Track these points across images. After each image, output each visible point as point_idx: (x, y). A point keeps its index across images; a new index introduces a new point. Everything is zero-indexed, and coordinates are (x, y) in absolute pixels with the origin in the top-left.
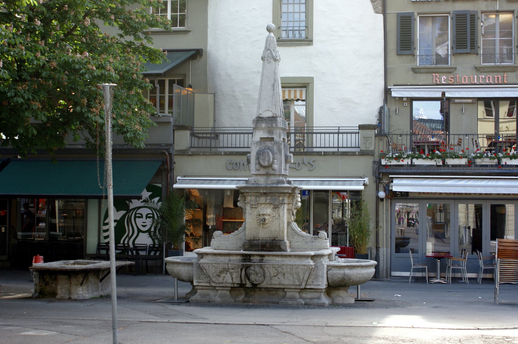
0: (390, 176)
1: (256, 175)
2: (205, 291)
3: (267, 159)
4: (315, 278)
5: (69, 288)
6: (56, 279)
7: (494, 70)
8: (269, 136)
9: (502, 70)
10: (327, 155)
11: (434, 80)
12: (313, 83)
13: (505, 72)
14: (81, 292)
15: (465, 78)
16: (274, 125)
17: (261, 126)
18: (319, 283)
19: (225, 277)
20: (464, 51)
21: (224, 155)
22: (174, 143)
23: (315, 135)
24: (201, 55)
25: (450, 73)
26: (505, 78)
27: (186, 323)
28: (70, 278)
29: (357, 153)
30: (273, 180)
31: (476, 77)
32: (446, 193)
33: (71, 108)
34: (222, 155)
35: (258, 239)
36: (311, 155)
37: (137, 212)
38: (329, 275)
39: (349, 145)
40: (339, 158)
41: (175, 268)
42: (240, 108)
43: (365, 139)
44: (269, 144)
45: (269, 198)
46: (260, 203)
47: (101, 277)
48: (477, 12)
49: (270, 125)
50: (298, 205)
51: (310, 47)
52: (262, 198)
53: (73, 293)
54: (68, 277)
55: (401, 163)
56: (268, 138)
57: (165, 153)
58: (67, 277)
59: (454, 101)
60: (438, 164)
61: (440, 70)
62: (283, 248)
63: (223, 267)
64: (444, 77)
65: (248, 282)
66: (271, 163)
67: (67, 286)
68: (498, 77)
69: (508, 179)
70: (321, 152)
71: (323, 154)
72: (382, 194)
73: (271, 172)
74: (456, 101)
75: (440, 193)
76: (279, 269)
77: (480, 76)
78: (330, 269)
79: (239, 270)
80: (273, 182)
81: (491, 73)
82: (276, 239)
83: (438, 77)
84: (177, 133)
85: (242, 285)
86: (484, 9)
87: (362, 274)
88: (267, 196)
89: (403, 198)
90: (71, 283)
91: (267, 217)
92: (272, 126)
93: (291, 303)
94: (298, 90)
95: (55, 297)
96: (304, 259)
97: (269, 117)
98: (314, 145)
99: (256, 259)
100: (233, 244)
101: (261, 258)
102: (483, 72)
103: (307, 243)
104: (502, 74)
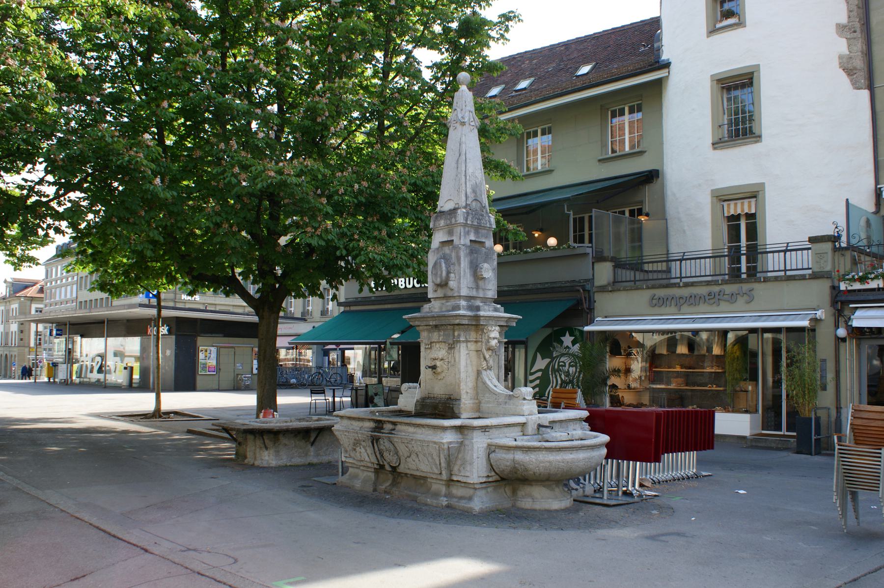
0: (851, 306)
3: (439, 273)
4: (461, 465)
10: (767, 281)
12: (764, 190)
14: (267, 458)
18: (468, 474)
21: (763, 282)
22: (593, 279)
24: (658, 177)
29: (807, 277)
37: (561, 360)
38: (492, 461)
39: (800, 267)
40: (784, 284)
42: (684, 231)
43: (819, 255)
45: (442, 333)
47: (312, 439)
50: (491, 344)
51: (758, 144)
55: (866, 286)
57: (579, 291)
66: (444, 278)
73: (450, 293)
78: (494, 451)
84: (597, 266)
87: (550, 462)
88: (439, 331)
91: (438, 363)
94: (746, 202)
98: (788, 267)
99: (388, 427)
103: (499, 404)
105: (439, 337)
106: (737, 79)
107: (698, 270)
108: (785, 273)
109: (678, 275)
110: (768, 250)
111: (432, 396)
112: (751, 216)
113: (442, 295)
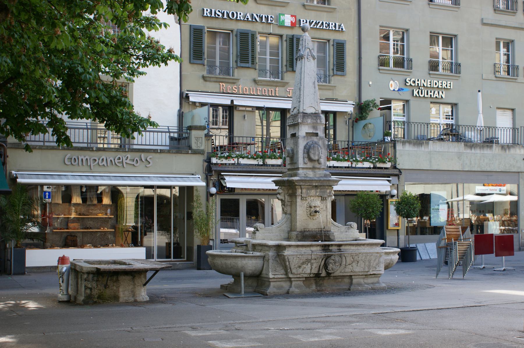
1: (303, 168)
2: (278, 283)
3: (317, 153)
6: (117, 280)
7: (269, 84)
8: (314, 132)
9: (275, 84)
11: (221, 89)
13: (277, 86)
15: (265, 90)
17: (307, 121)
19: (305, 268)
20: (247, 65)
25: (234, 83)
26: (277, 91)
27: (413, 311)
28: (134, 277)
30: (320, 174)
31: (254, 88)
32: (263, 189)
34: (60, 149)
35: (308, 230)
36: (148, 152)
39: (160, 144)
41: (239, 262)
44: (315, 139)
45: (319, 190)
46: (311, 195)
48: (255, 32)
49: (314, 121)
52: (313, 191)
53: (138, 295)
54: (131, 277)
56: (313, 133)
59: (238, 108)
60: (259, 164)
61: (227, 80)
62: (332, 238)
63: (306, 258)
64: (229, 86)
65: (324, 271)
68: (272, 91)
69: (255, 176)
71: (159, 151)
72: (213, 190)
73: (317, 166)
74: (241, 108)
75: (259, 189)
76: (356, 257)
77: (258, 89)
79: (320, 261)
80: (321, 175)
81: (266, 87)
83: (224, 86)
85: (317, 276)
86: (261, 30)
88: (317, 189)
89: (231, 193)
90: (134, 285)
92: (317, 122)
93: (361, 289)
95: (119, 301)
96: (374, 247)
97: (312, 113)
100: (277, 236)
101: (338, 248)
102: (261, 85)
104: (274, 88)
107: (81, 138)
108: (44, 144)
110: (98, 127)
112: (240, 33)
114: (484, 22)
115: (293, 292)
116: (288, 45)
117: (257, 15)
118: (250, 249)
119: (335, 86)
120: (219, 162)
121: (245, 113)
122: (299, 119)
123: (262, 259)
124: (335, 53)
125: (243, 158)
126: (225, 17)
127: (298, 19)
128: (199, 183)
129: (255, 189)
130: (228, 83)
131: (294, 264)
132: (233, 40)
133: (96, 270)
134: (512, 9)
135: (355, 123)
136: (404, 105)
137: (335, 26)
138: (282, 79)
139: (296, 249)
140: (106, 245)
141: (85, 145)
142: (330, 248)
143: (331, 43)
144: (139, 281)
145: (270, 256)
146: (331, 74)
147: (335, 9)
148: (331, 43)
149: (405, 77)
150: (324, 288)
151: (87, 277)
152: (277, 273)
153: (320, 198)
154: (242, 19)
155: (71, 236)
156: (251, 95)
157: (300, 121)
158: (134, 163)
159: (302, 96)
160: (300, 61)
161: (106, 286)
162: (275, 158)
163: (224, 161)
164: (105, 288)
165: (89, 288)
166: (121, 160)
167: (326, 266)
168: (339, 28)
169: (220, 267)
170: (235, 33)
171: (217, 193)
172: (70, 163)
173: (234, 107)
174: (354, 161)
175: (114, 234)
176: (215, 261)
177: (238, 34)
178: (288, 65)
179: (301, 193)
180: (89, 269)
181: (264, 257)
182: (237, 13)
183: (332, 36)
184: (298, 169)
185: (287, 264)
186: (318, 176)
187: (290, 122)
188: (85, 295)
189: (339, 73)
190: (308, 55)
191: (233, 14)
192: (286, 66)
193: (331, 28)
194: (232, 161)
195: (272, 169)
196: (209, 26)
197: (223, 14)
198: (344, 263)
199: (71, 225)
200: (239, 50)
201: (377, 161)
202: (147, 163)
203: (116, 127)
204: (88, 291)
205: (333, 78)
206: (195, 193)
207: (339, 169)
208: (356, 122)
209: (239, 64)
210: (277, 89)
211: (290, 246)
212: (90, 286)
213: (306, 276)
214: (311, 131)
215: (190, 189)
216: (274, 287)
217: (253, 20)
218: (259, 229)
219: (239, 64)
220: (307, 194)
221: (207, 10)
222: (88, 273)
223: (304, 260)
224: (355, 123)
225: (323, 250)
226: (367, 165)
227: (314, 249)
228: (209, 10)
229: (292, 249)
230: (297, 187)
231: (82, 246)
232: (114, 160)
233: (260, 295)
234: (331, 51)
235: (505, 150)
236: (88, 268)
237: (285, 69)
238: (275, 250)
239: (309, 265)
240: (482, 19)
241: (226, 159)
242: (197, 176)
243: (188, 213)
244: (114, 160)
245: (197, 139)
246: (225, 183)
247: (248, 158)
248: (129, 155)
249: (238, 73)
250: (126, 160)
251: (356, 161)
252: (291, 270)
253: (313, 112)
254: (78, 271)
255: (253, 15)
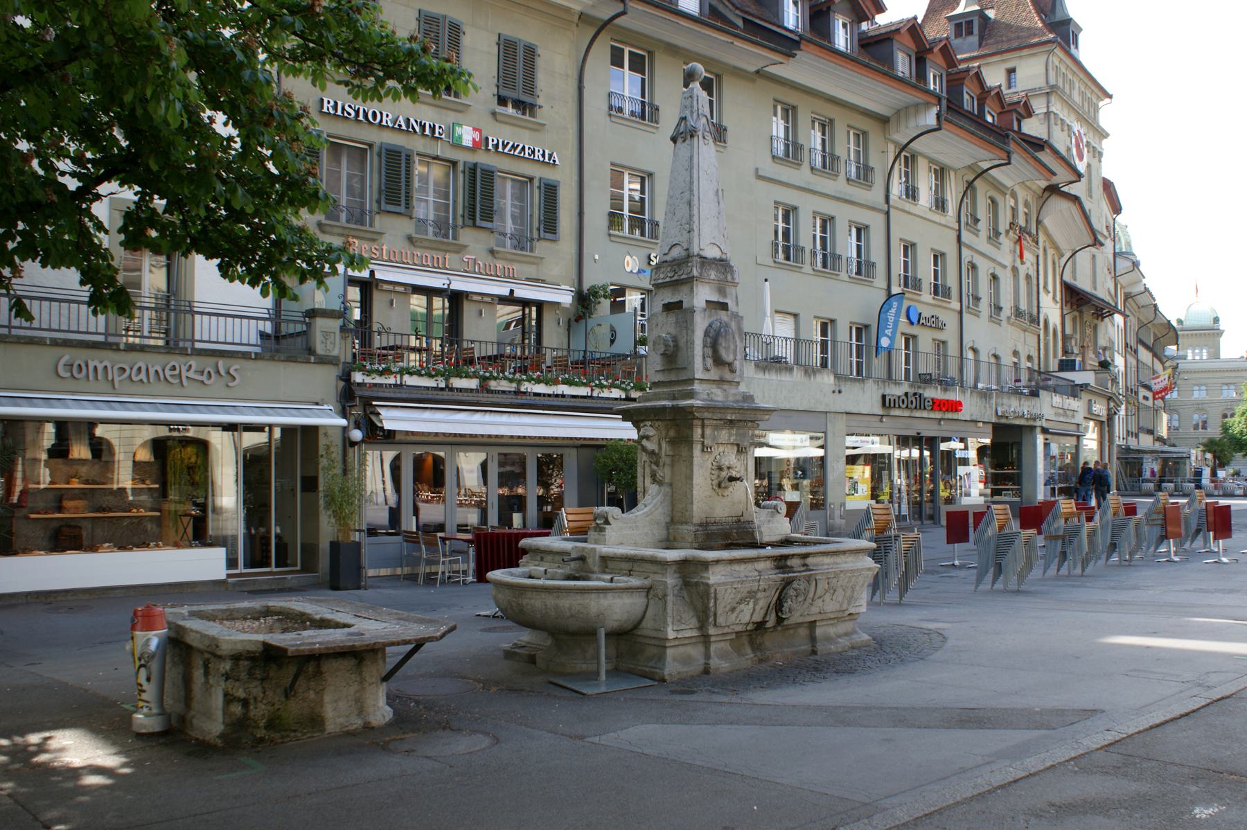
2: (681, 649)
3: (732, 347)
5: (358, 695)
6: (319, 673)
7: (434, 245)
8: (721, 300)
13: (446, 251)
16: (729, 278)
23: (197, 317)
25: (374, 240)
33: (189, 161)
34: (45, 344)
44: (723, 316)
45: (734, 432)
48: (412, 151)
58: (353, 661)
67: (355, 687)
70: (250, 353)
72: (357, 435)
73: (728, 376)
75: (437, 434)
76: (834, 580)
82: (742, 520)
85: (760, 626)
86: (421, 149)
88: (732, 428)
90: (362, 681)
95: (323, 730)
97: (715, 259)
98: (197, 337)
102: (421, 247)
105: (730, 437)
106: (451, 106)
108: (10, 332)
109: (190, 338)
111: (713, 520)
113: (717, 378)
114: (761, 173)
115: (717, 669)
116: (467, 179)
117: (416, 121)
118: (596, 569)
119: (542, 258)
120: (368, 380)
121: (393, 296)
122: (695, 269)
123: (644, 594)
124: (542, 202)
125: (411, 374)
126: (361, 117)
127: (484, 134)
128: (329, 419)
129: (430, 434)
130: (363, 238)
131: (723, 605)
132: (372, 162)
133: (261, 648)
134: (795, 157)
135: (573, 323)
136: (643, 299)
137: (543, 155)
138: (455, 238)
139: (728, 568)
140: (144, 545)
141: (101, 338)
142: (789, 563)
143: (536, 183)
144: (373, 671)
145: (669, 586)
146: (536, 235)
147: (543, 125)
148: (536, 183)
149: (648, 251)
150: (768, 653)
151: (232, 669)
152: (683, 627)
153: (735, 448)
154: (390, 125)
155: (70, 526)
156: (401, 264)
157: (695, 273)
158: (204, 378)
159: (696, 219)
160: (688, 141)
161: (289, 692)
162: (466, 377)
163: (378, 380)
164: (287, 696)
165: (239, 700)
166: (177, 372)
167: (779, 605)
168: (550, 159)
169: (539, 616)
170: (376, 149)
171: (363, 441)
172: (69, 374)
173: (374, 283)
174: (596, 386)
175: (158, 521)
176: (525, 602)
177: (383, 151)
178: (466, 215)
179: (703, 436)
180: (240, 647)
181: (648, 590)
182: (381, 114)
183: (537, 172)
184: (691, 381)
185: (712, 604)
186: (731, 398)
187: (662, 276)
188: (228, 720)
189: (548, 236)
190: (705, 130)
191: (374, 114)
192: (463, 216)
193: (536, 158)
194: (391, 380)
195: (461, 396)
196: (332, 131)
197: (357, 112)
198: (811, 595)
199: (68, 504)
200: (383, 181)
201: (632, 388)
202: (230, 378)
203: (249, 270)
204: (237, 709)
205: (538, 245)
206: (322, 441)
207: (542, 398)
208: (577, 321)
209: (384, 206)
210: (447, 257)
211: (717, 562)
212: (241, 693)
213: (739, 628)
214: (715, 298)
215: (310, 432)
216: (675, 660)
217: (409, 130)
218: (610, 519)
219: (384, 206)
220: (714, 438)
221: (329, 102)
222: (236, 658)
223: (745, 594)
224: (573, 323)
225: (777, 568)
226: (616, 393)
227: (761, 566)
228: (332, 103)
229: (719, 569)
230: (695, 422)
231: (93, 548)
232: (164, 370)
233: (650, 683)
234: (535, 197)
235: (810, 376)
236: (235, 642)
237: (460, 222)
238: (675, 572)
239: (751, 604)
240: (757, 169)
241: (381, 375)
242: (325, 407)
243: (304, 479)
244: (164, 370)
245: (326, 334)
246: (381, 422)
247: (420, 375)
248: (194, 362)
249: (380, 222)
250: (188, 371)
251: (601, 386)
252: (715, 620)
253: (718, 257)
254: (189, 648)
255: (408, 120)
